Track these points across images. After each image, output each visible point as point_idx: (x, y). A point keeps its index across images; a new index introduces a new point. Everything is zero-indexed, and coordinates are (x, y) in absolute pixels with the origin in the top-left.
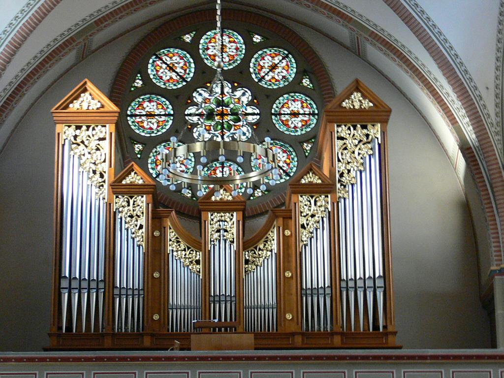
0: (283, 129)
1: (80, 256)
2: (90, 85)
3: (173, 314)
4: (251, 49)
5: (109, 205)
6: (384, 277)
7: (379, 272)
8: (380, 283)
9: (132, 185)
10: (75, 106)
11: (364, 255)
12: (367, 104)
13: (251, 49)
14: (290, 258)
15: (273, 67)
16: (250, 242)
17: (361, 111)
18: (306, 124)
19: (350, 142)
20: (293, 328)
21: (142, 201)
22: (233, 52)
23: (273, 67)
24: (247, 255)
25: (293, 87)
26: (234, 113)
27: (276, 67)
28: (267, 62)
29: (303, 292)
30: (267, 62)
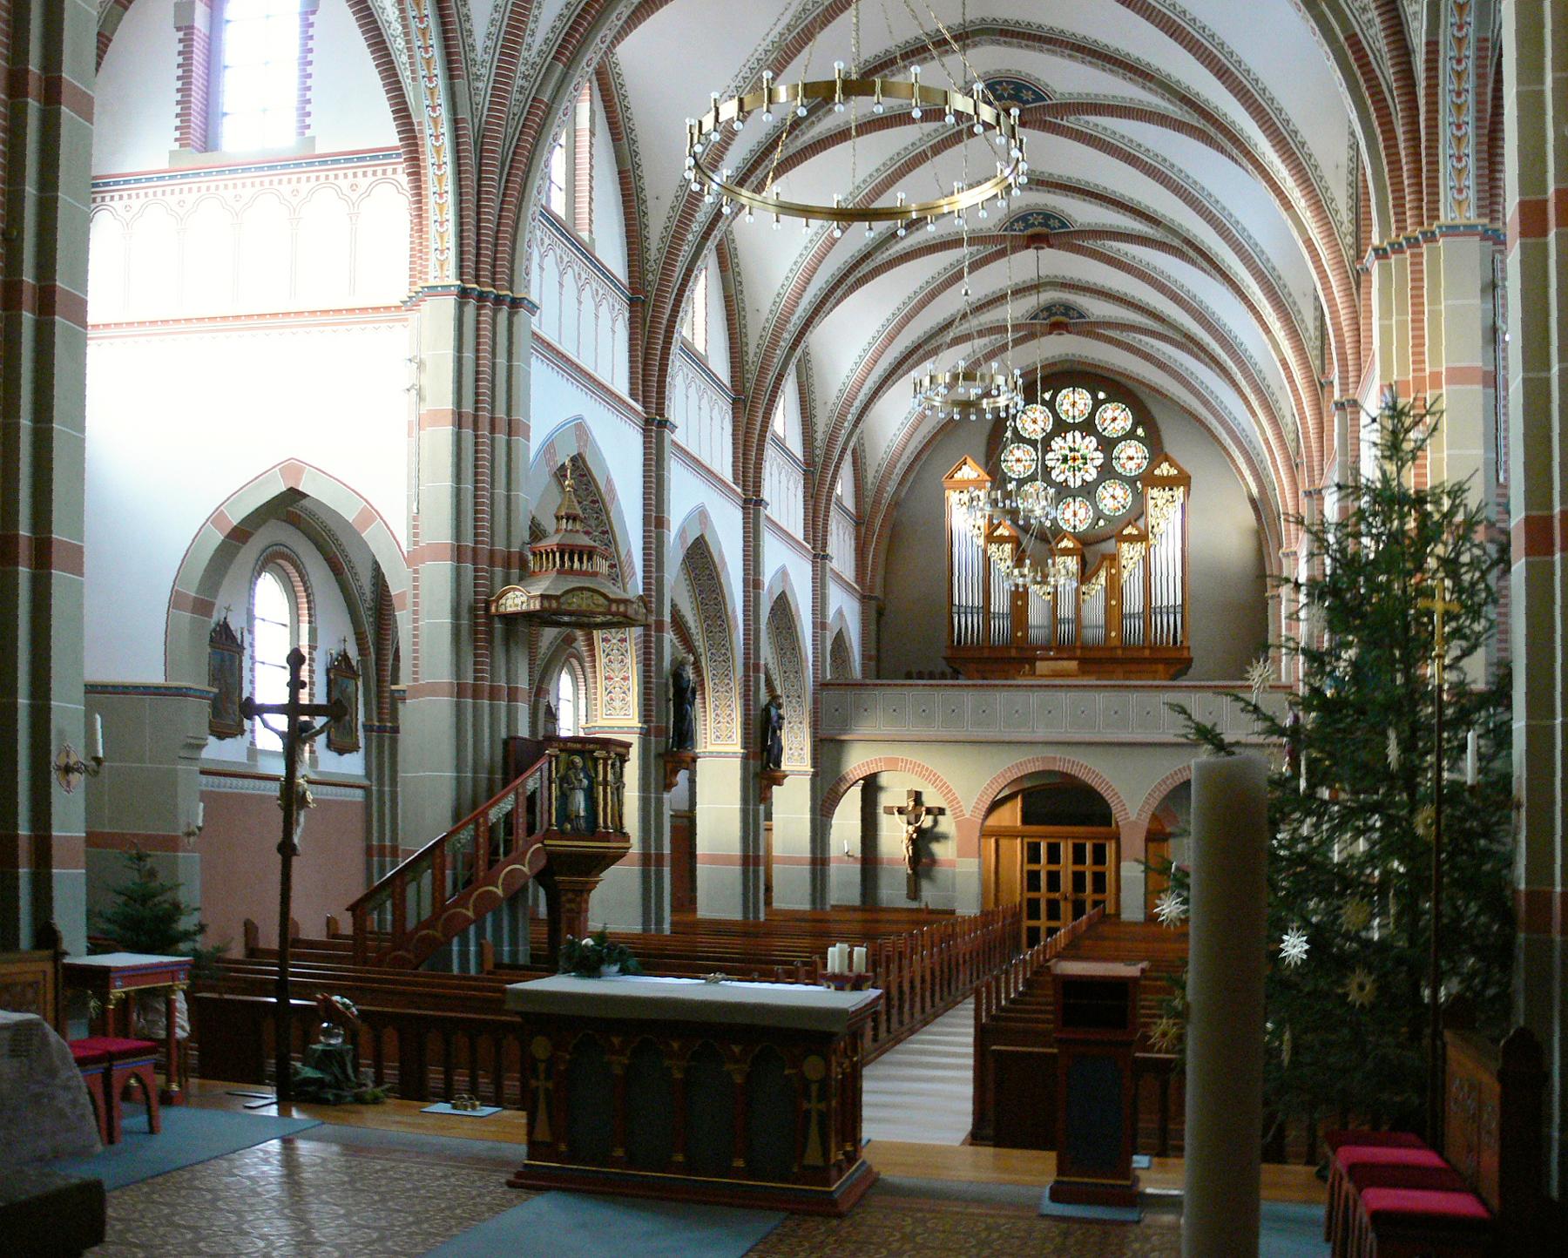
0: (1120, 470)
1: (966, 593)
2: (969, 460)
3: (1033, 633)
4: (1097, 403)
5: (985, 551)
6: (1182, 605)
7: (1179, 602)
8: (1179, 610)
9: (1001, 536)
10: (958, 476)
11: (1169, 592)
12: (1173, 472)
13: (1097, 403)
14: (1114, 590)
15: (1114, 419)
16: (1085, 575)
17: (1169, 477)
18: (1139, 466)
19: (1160, 502)
20: (1116, 643)
21: (1008, 547)
22: (1082, 407)
23: (1114, 419)
24: (1084, 589)
25: (1130, 435)
26: (1084, 458)
27: (1116, 418)
28: (1109, 415)
29: (1123, 616)
30: (1109, 415)
